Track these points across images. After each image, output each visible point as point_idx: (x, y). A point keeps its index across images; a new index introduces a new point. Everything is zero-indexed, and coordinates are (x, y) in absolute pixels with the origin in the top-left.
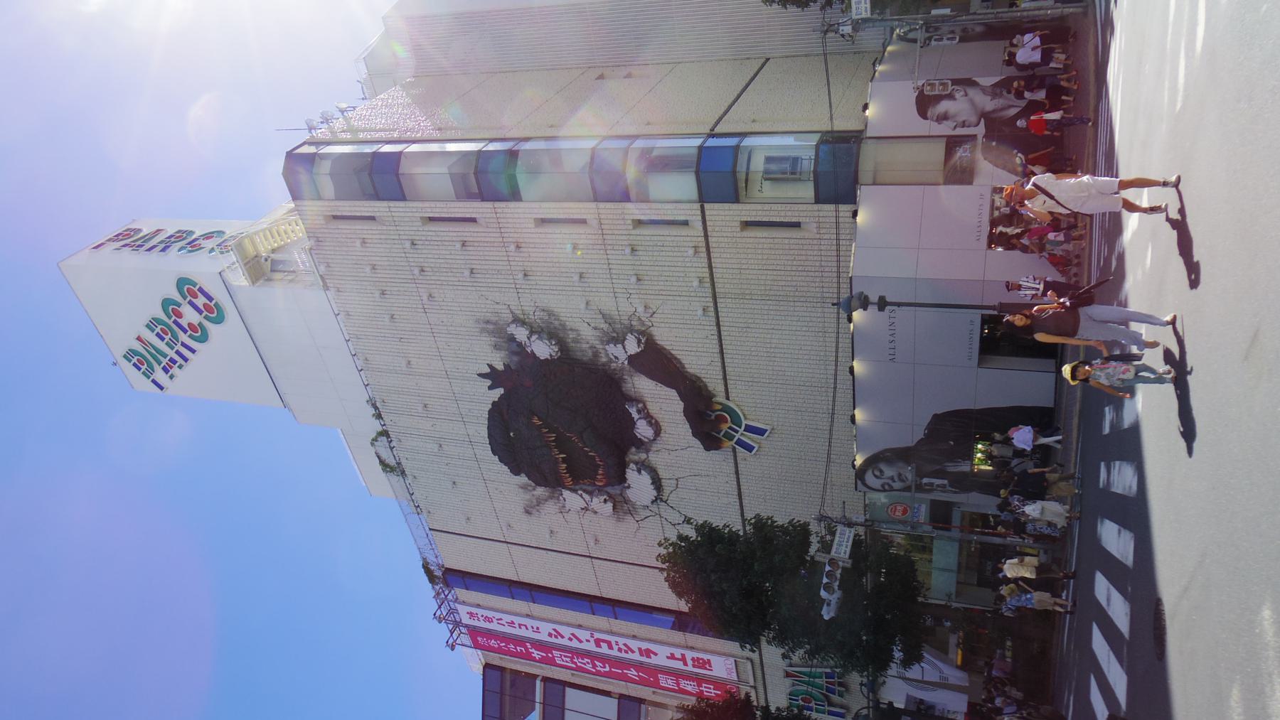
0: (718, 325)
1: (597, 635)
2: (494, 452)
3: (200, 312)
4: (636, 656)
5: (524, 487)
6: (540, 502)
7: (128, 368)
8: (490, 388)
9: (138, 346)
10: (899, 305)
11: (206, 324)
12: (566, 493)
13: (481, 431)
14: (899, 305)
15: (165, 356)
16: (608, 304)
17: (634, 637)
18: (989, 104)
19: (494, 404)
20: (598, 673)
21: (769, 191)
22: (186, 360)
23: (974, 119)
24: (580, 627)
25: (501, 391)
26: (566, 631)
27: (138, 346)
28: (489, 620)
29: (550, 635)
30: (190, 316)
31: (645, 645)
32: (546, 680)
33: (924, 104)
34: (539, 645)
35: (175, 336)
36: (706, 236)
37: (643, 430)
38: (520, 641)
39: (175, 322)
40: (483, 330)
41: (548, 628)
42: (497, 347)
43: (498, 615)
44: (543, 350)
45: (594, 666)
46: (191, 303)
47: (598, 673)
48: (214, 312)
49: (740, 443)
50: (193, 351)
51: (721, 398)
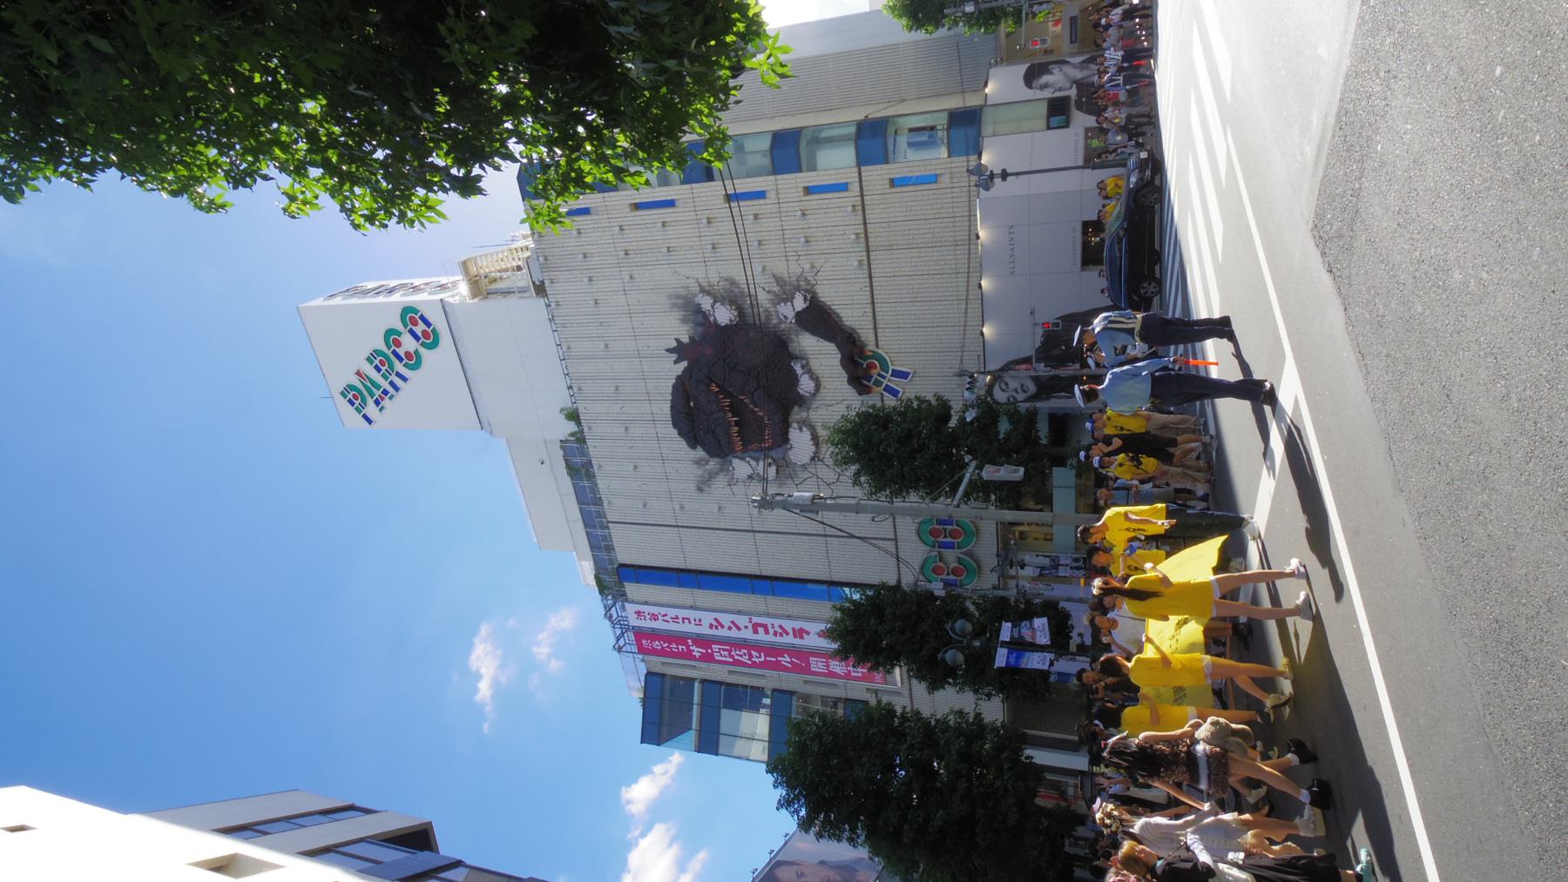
0: (870, 277)
1: (756, 620)
2: (675, 425)
3: (417, 338)
4: (789, 639)
5: (698, 462)
6: (712, 476)
7: (343, 403)
8: (676, 362)
9: (355, 381)
10: (1017, 174)
11: (422, 351)
12: (736, 462)
13: (664, 408)
14: (1017, 174)
15: (378, 387)
16: (780, 267)
17: (789, 617)
18: (1078, 74)
19: (678, 378)
20: (754, 665)
21: (912, 155)
22: (397, 389)
23: (1067, 85)
24: (739, 612)
25: (684, 364)
26: (726, 619)
27: (355, 381)
28: (654, 617)
29: (711, 626)
30: (409, 344)
31: (798, 625)
32: (704, 682)
33: (1030, 78)
34: (703, 641)
35: (391, 367)
36: (862, 196)
37: (806, 385)
38: (681, 639)
39: (394, 353)
40: (674, 305)
41: (708, 618)
42: (684, 321)
43: (663, 610)
44: (724, 315)
45: (751, 657)
46: (412, 332)
47: (754, 665)
48: (430, 339)
49: (888, 389)
50: (404, 379)
51: (871, 347)
